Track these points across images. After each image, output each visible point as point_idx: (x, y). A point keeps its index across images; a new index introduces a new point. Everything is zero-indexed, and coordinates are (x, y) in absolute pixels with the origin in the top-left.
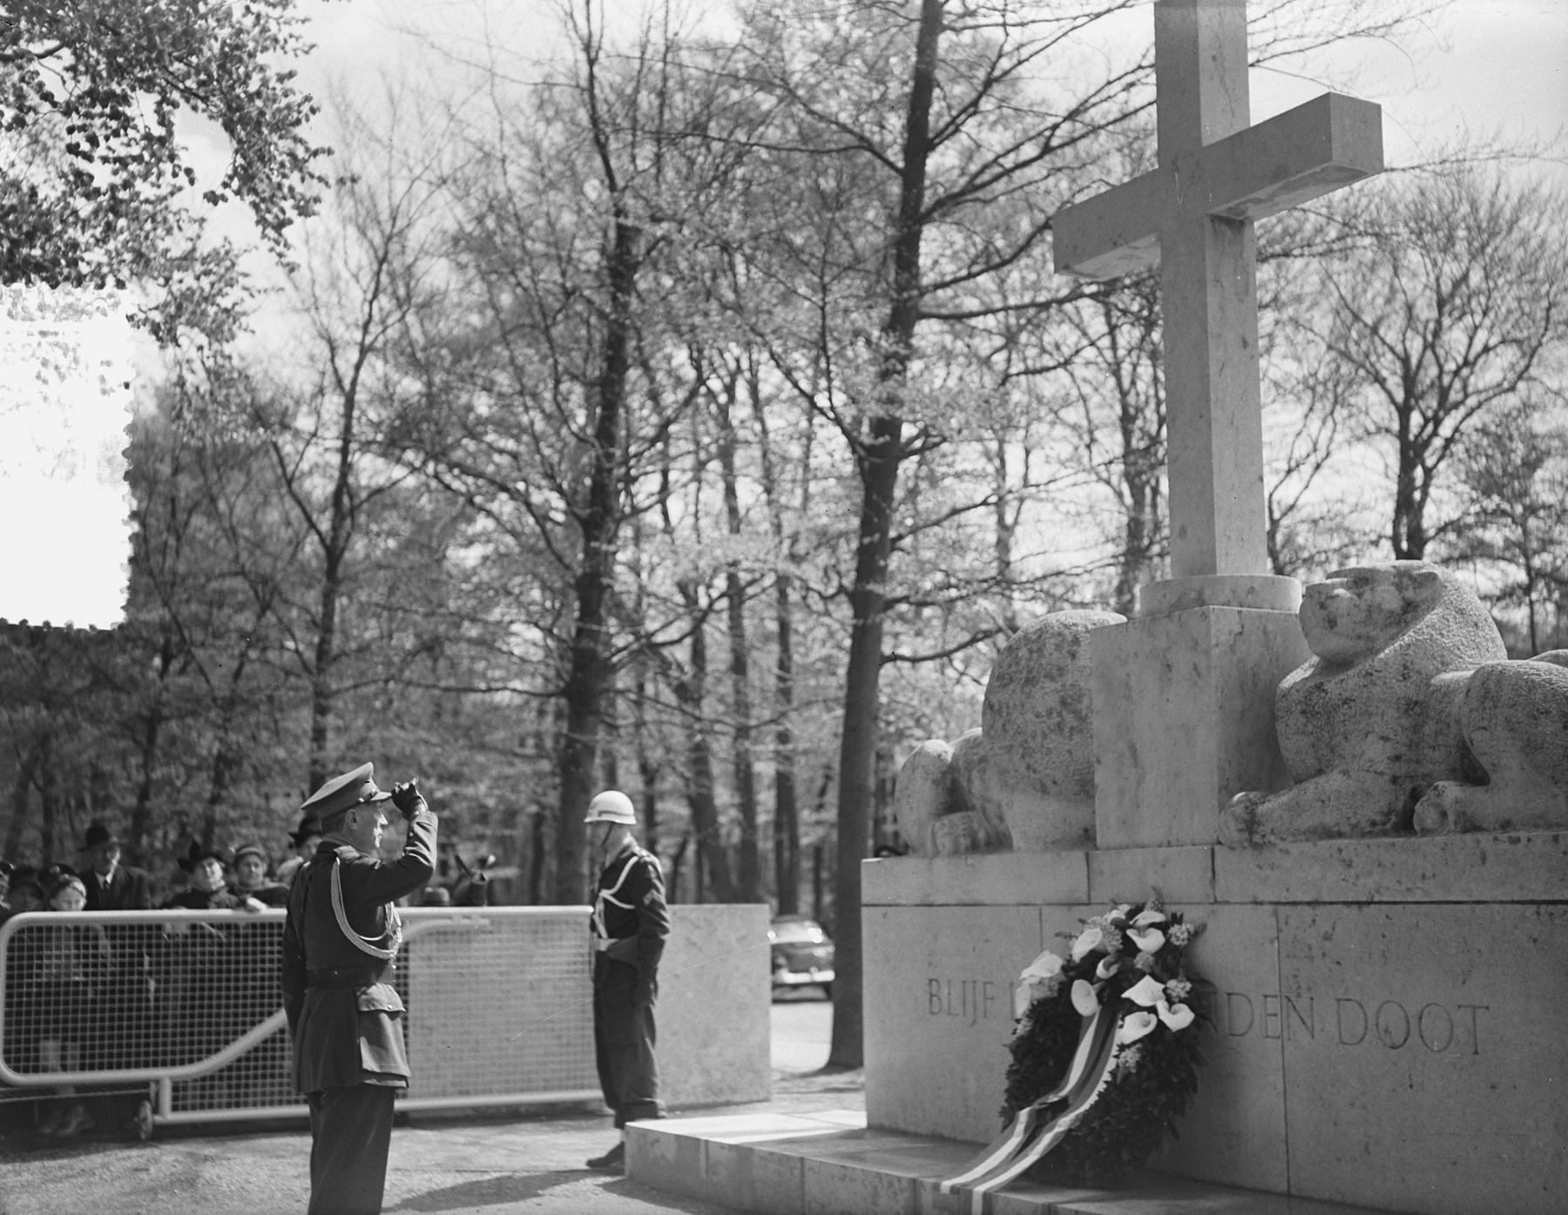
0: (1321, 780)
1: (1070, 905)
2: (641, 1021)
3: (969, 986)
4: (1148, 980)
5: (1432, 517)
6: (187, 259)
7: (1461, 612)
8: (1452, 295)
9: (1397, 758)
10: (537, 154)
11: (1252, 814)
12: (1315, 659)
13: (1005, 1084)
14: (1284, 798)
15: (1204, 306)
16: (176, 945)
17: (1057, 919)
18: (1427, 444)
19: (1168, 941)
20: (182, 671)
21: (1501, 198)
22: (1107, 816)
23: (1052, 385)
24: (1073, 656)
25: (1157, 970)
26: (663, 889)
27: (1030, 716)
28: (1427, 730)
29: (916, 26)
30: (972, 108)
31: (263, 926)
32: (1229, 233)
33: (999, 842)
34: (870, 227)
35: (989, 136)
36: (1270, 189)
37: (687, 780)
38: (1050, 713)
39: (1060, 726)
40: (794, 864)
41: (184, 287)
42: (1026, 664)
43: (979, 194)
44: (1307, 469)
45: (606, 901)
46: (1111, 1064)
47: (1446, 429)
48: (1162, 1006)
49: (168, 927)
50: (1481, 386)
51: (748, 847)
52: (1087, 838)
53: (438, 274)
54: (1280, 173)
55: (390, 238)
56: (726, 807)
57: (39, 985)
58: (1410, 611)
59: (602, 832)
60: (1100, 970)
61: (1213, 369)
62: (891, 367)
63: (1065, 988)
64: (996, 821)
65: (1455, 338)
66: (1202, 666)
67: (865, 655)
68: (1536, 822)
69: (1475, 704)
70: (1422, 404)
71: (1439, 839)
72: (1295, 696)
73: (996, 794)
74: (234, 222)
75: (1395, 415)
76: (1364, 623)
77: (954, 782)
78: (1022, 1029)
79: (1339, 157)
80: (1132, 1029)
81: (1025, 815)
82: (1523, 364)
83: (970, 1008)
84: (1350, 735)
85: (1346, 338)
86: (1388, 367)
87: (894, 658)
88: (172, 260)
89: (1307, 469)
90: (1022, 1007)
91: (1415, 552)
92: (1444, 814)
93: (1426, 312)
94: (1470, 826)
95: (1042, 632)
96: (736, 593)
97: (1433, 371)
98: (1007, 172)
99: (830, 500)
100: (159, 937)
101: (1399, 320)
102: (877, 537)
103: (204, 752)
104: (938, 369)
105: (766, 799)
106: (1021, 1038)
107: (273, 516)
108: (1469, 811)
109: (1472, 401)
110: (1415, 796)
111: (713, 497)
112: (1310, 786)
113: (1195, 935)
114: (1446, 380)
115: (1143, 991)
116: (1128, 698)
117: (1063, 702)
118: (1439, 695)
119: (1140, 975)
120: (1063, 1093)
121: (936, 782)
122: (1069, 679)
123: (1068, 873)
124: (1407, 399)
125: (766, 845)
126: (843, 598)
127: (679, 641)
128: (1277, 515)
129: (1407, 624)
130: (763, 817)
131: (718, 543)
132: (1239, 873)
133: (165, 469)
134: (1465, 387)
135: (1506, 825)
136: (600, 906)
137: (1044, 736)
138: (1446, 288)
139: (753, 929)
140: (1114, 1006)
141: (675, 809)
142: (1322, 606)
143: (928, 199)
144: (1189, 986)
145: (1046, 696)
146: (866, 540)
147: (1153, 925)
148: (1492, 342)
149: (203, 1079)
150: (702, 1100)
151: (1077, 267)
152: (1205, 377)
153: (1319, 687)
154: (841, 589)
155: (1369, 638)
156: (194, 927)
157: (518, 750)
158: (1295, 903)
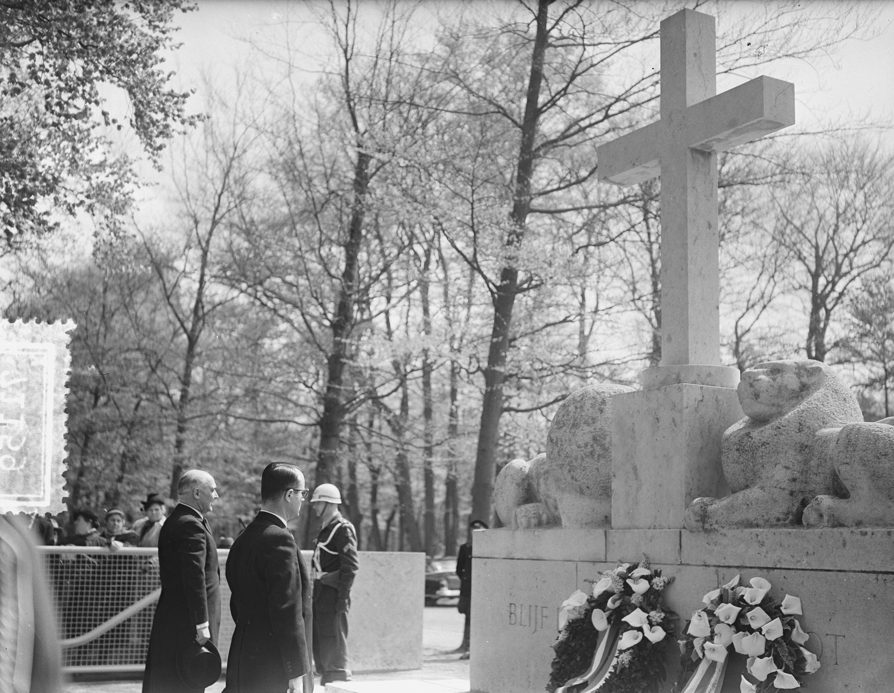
0: (747, 491)
1: (594, 562)
2: (339, 622)
3: (533, 608)
4: (638, 610)
5: (829, 337)
6: (101, 166)
7: (836, 392)
8: (845, 212)
9: (794, 480)
10: (320, 117)
11: (705, 510)
12: (746, 418)
13: (551, 670)
14: (725, 502)
15: (686, 202)
16: (68, 567)
17: (587, 570)
18: (828, 295)
19: (651, 586)
20: (105, 404)
21: (877, 156)
22: (618, 509)
23: (611, 252)
24: (601, 411)
25: (644, 605)
26: (355, 543)
27: (574, 447)
28: (812, 463)
29: (533, 44)
30: (564, 92)
31: (120, 557)
32: (701, 159)
33: (554, 522)
34: (506, 163)
35: (574, 108)
36: (726, 133)
37: (394, 474)
38: (586, 445)
39: (592, 454)
40: (456, 526)
41: (99, 181)
42: (573, 414)
43: (567, 141)
44: (758, 308)
45: (321, 549)
46: (614, 662)
47: (839, 288)
48: (646, 627)
49: (63, 555)
50: (860, 264)
51: (429, 517)
52: (606, 521)
53: (261, 183)
54: (733, 124)
55: (232, 159)
56: (418, 493)
57: (83, 573)
58: (804, 389)
59: (320, 508)
60: (610, 604)
61: (690, 241)
62: (516, 236)
63: (588, 613)
64: (553, 510)
65: (847, 236)
66: (678, 420)
67: (492, 405)
68: (879, 522)
69: (842, 448)
70: (826, 273)
71: (818, 531)
72: (733, 439)
73: (555, 494)
74: (130, 142)
75: (810, 278)
76: (777, 397)
77: (529, 485)
78: (562, 637)
79: (767, 114)
80: (627, 640)
81: (570, 506)
82: (885, 250)
83: (533, 621)
84: (761, 465)
85: (783, 234)
86: (807, 251)
87: (509, 409)
88: (92, 166)
89: (758, 308)
90: (563, 624)
91: (820, 357)
92: (821, 516)
93: (830, 217)
94: (837, 523)
95: (583, 396)
96: (427, 369)
97: (833, 255)
98: (582, 129)
99: (480, 318)
100: (57, 562)
101: (814, 224)
102: (501, 338)
103: (115, 451)
104: (541, 240)
105: (440, 488)
106: (561, 643)
107: (160, 318)
108: (837, 514)
109: (855, 272)
110: (804, 503)
111: (417, 314)
112: (740, 495)
113: (669, 583)
114: (840, 259)
115: (635, 618)
116: (634, 438)
117: (595, 439)
118: (820, 442)
119: (634, 608)
120: (586, 678)
121: (518, 485)
122: (598, 425)
123: (592, 542)
124: (817, 270)
125: (439, 514)
126: (479, 373)
127: (395, 390)
128: (739, 333)
129: (803, 398)
130: (439, 499)
131: (417, 341)
132: (696, 547)
133: (100, 289)
134: (851, 264)
135: (859, 524)
136: (318, 553)
137: (583, 459)
138: (842, 206)
139: (409, 568)
140: (618, 626)
141: (388, 492)
142: (751, 385)
143: (538, 142)
144: (663, 615)
145: (584, 435)
146: (495, 340)
147: (643, 577)
148: (868, 238)
149: (80, 647)
150: (380, 668)
151: (611, 178)
152: (685, 245)
153: (748, 435)
154: (479, 369)
155: (779, 406)
156: (78, 556)
157: (302, 456)
158: (729, 567)
